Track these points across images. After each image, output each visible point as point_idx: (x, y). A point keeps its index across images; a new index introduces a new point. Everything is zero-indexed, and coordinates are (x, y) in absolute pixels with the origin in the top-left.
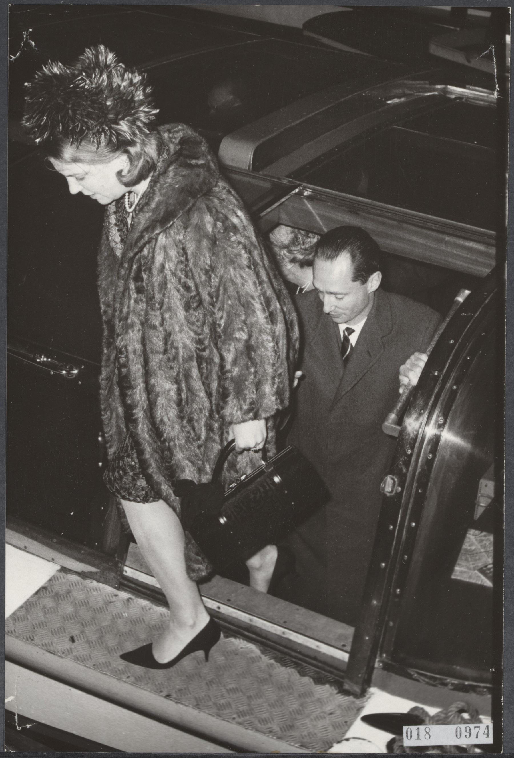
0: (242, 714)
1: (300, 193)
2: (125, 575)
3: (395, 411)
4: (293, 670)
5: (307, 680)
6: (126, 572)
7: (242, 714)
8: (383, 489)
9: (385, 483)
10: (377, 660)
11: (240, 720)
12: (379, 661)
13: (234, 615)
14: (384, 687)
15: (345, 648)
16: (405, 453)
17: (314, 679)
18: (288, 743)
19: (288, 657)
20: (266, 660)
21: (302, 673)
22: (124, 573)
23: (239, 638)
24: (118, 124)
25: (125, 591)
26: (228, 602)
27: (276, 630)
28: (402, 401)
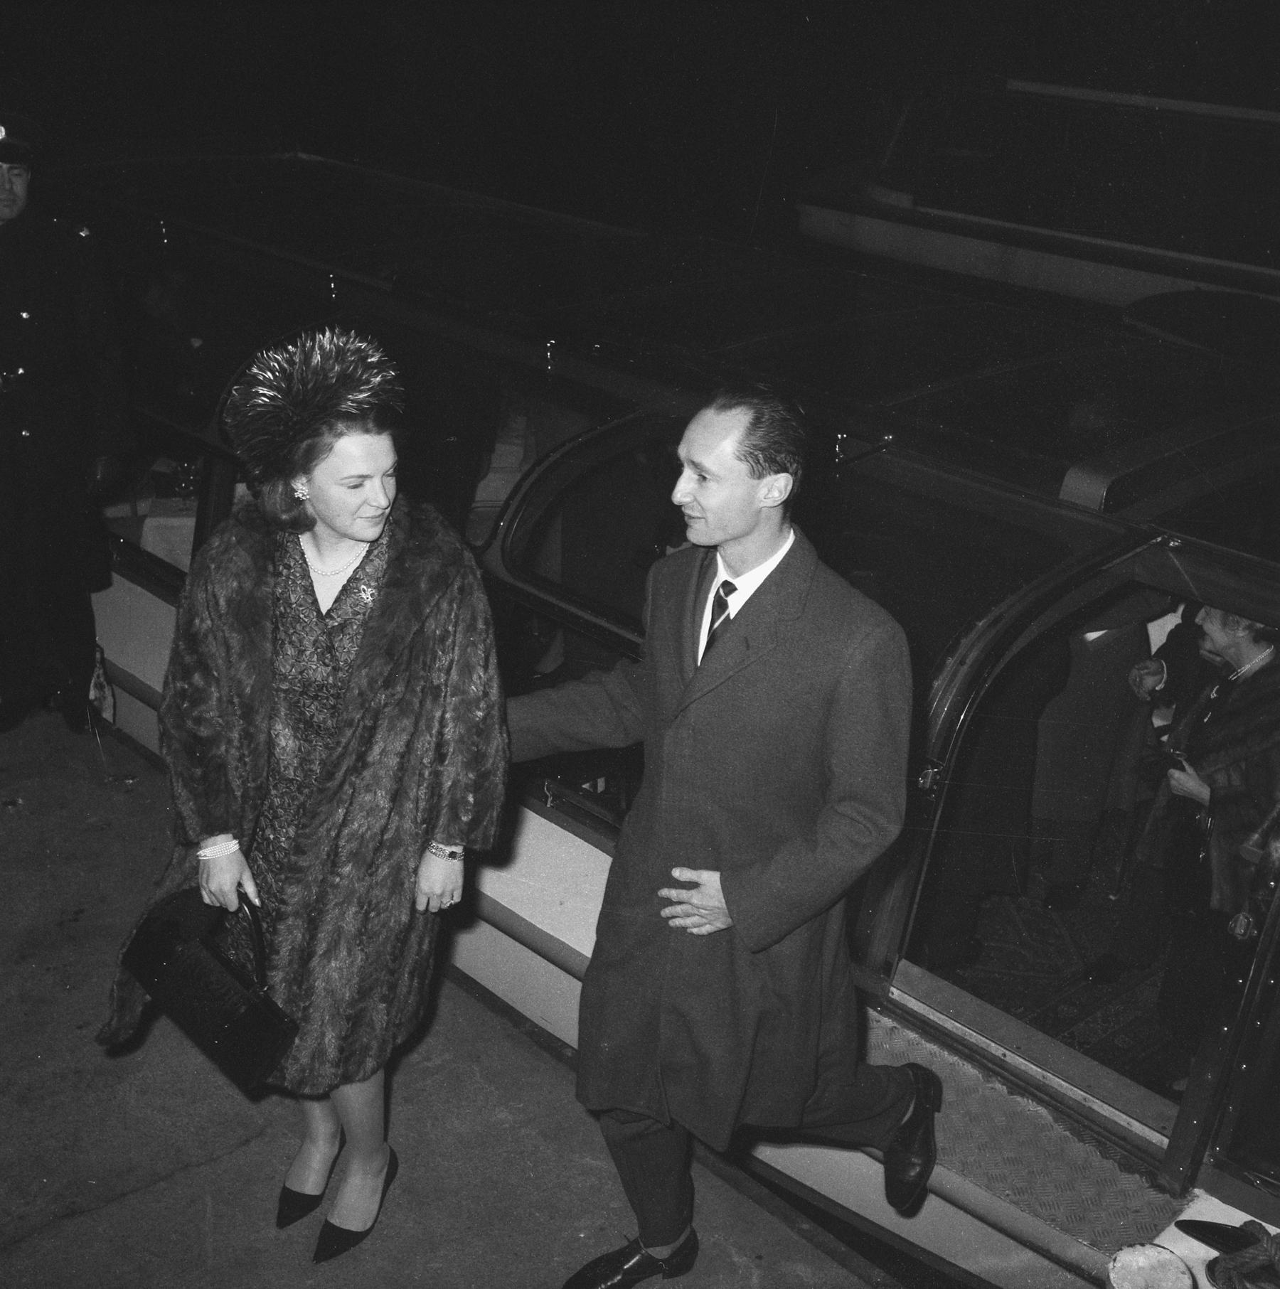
0: (1020, 1192)
1: (1165, 543)
2: (890, 997)
3: (1260, 830)
4: (1093, 1149)
5: (1109, 1164)
6: (893, 994)
7: (1020, 1192)
8: (1233, 930)
9: (1236, 922)
10: (1207, 1153)
11: (1015, 1199)
12: (1211, 1156)
13: (1023, 1068)
14: (1212, 1191)
15: (1165, 1132)
16: (1268, 886)
17: (1120, 1164)
18: (1075, 1237)
19: (1088, 1131)
20: (1060, 1130)
21: (1105, 1155)
22: (890, 995)
23: (1028, 1098)
24: (1244, 629)
25: (889, 1017)
26: (1018, 1051)
27: (1077, 1094)
28: (1270, 818)
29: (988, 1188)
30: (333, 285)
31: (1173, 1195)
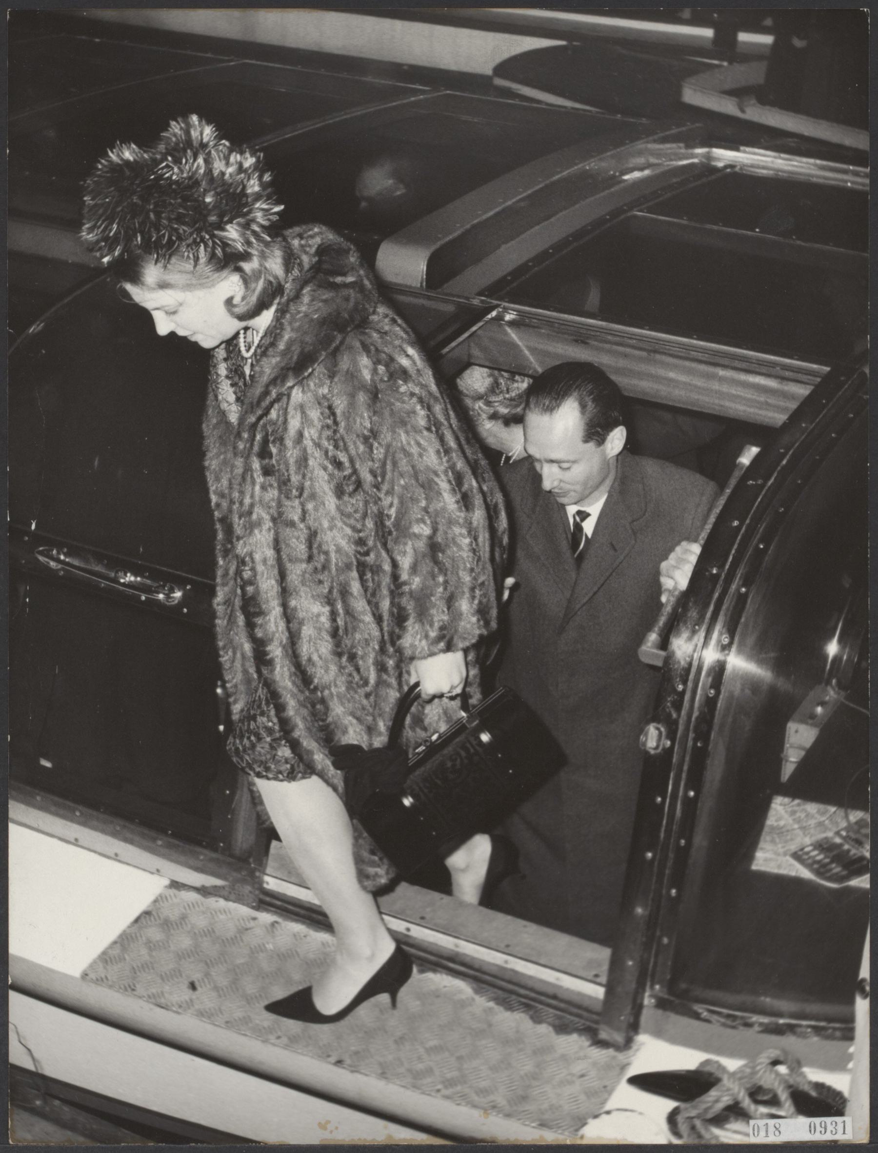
0: (449, 1083)
1: (500, 318)
3: (656, 629)
6: (268, 883)
8: (644, 744)
9: (646, 735)
14: (658, 1033)
15: (598, 980)
16: (675, 690)
19: (514, 997)
20: (482, 1003)
21: (537, 1019)
25: (267, 911)
28: (665, 614)
29: (415, 1087)
30: (48, 764)
31: (619, 1048)
